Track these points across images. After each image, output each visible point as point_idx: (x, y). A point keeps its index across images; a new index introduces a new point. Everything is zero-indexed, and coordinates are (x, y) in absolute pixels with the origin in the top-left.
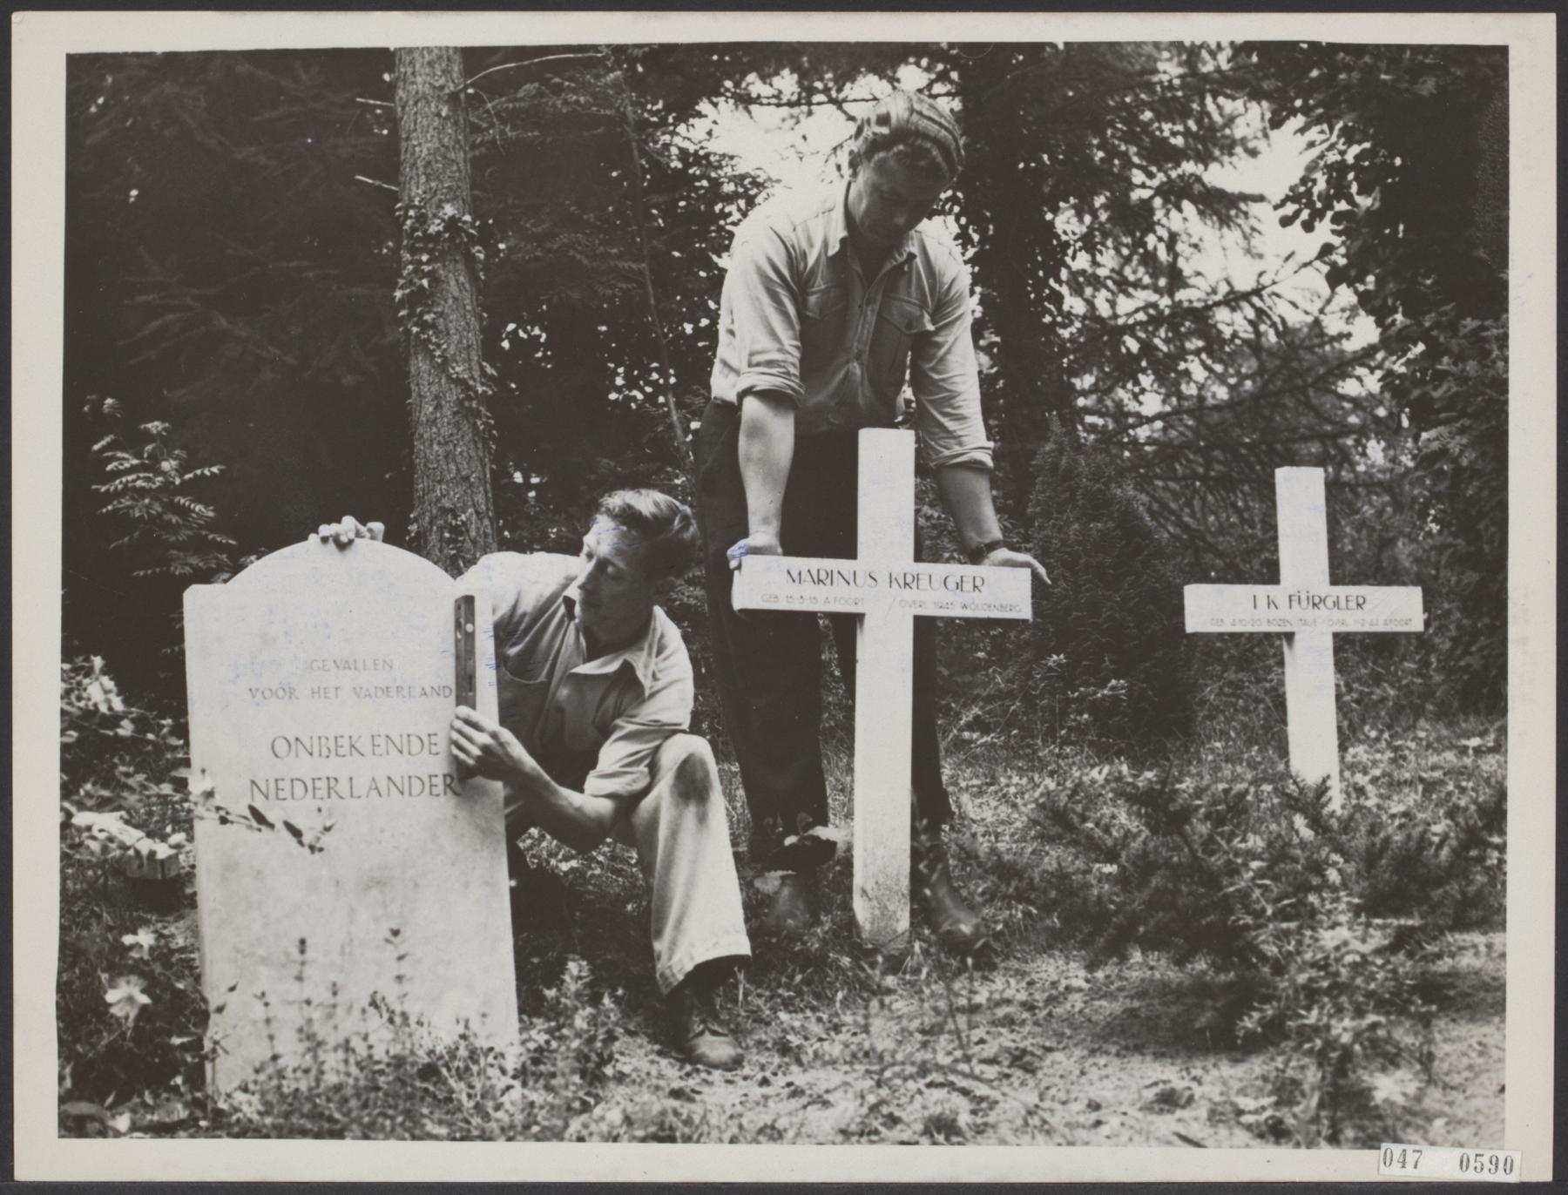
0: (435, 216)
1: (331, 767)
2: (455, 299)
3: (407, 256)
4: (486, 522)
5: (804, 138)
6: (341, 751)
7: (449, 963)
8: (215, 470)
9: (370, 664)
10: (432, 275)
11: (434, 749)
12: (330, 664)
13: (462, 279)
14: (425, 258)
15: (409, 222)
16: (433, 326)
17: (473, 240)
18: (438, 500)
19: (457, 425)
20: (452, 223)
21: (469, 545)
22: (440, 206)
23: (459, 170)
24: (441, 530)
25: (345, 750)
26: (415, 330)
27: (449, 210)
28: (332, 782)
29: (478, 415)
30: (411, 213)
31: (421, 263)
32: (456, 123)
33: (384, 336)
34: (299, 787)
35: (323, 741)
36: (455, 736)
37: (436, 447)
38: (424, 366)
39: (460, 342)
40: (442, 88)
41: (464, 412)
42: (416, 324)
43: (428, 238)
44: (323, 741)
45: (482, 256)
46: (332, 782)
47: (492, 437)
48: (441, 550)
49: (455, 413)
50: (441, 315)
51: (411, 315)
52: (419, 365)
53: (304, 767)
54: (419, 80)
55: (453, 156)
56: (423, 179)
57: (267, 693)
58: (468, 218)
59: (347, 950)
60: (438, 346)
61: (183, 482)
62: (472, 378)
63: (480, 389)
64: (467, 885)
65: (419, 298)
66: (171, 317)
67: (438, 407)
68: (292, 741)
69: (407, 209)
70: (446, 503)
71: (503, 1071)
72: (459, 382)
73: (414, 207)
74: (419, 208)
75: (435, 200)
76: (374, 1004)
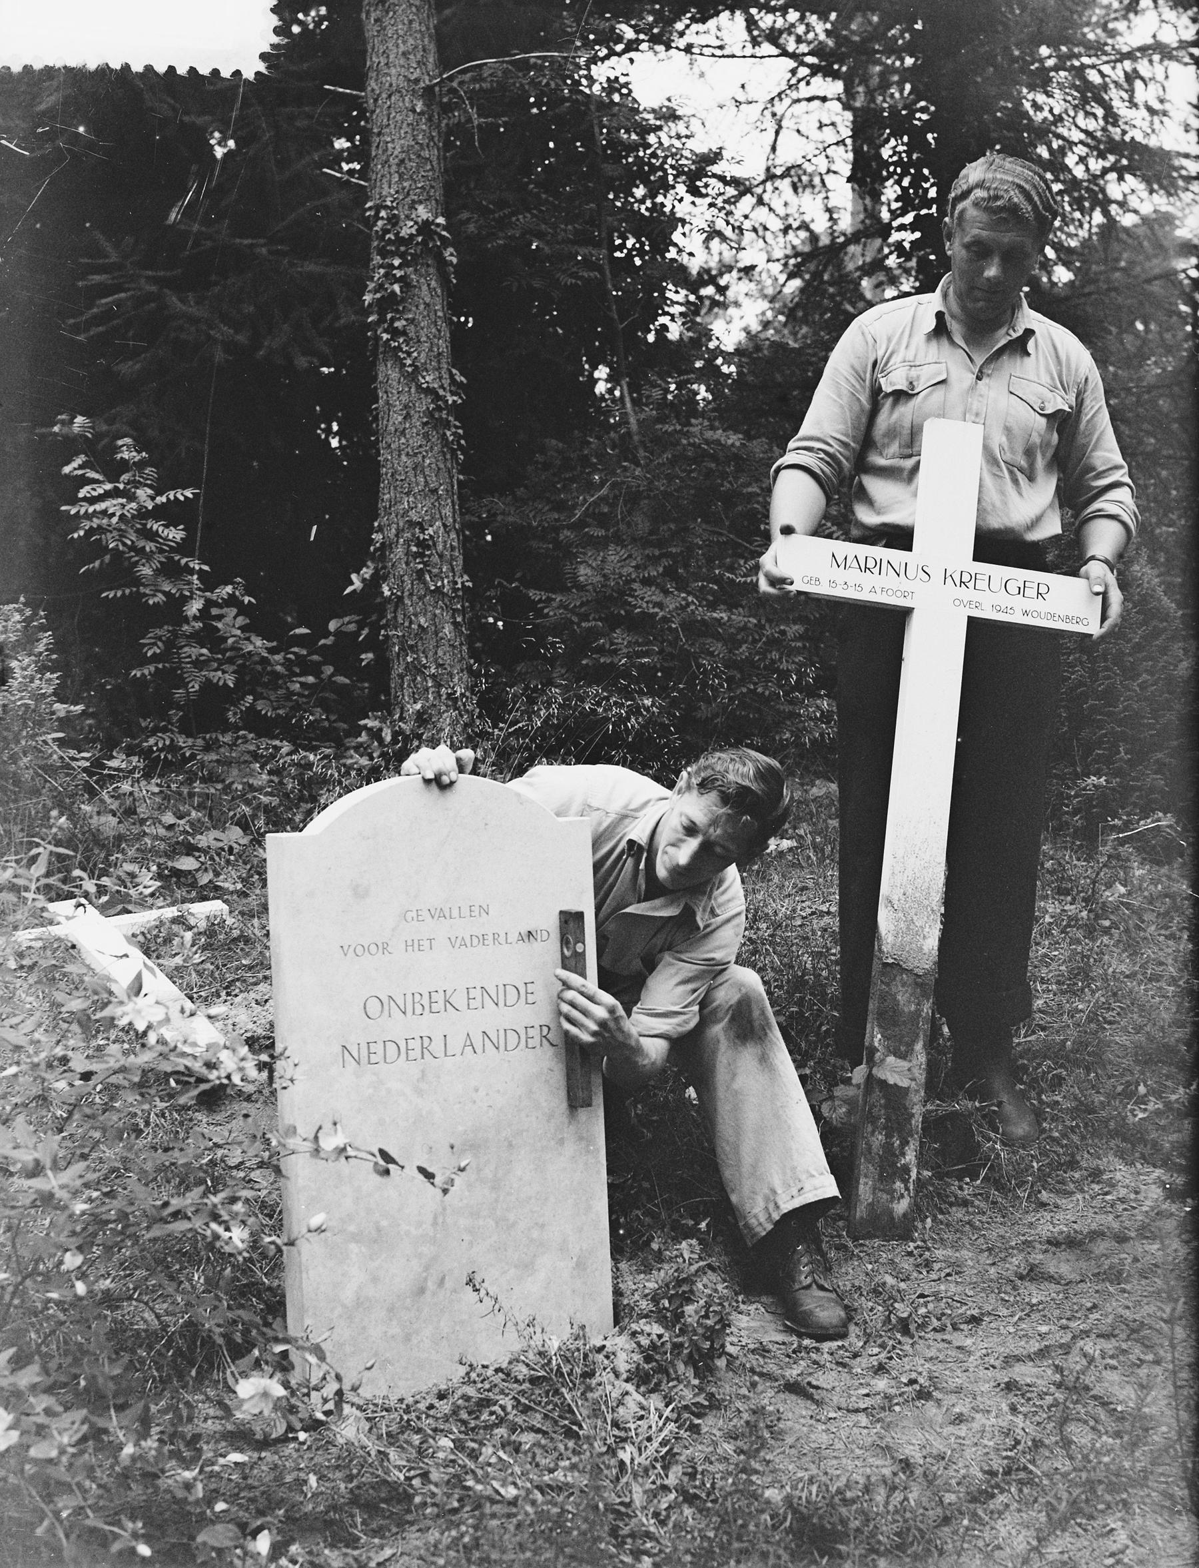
0: (408, 217)
1: (425, 1025)
2: (427, 305)
3: (377, 259)
4: (453, 535)
5: (743, 86)
6: (435, 1007)
7: (543, 1226)
8: (189, 493)
9: (465, 911)
10: (403, 280)
11: (531, 999)
12: (425, 914)
13: (433, 284)
14: (397, 262)
15: (380, 223)
16: (404, 333)
17: (445, 242)
18: (406, 512)
19: (426, 436)
20: (425, 228)
21: (436, 559)
22: (412, 207)
23: (432, 169)
24: (407, 543)
25: (439, 1006)
26: (385, 336)
27: (423, 213)
28: (426, 1040)
29: (447, 425)
30: (383, 214)
31: (392, 267)
32: (430, 119)
33: (338, 317)
34: (392, 1048)
35: (417, 997)
36: (565, 1008)
37: (404, 458)
38: (394, 375)
39: (431, 350)
40: (417, 81)
41: (434, 422)
42: (385, 331)
43: (400, 240)
44: (417, 997)
45: (455, 260)
46: (426, 1040)
47: (460, 446)
48: (407, 564)
49: (425, 424)
50: (411, 321)
51: (382, 320)
52: (388, 373)
53: (398, 1027)
54: (393, 71)
55: (426, 154)
56: (396, 178)
57: (359, 950)
58: (441, 220)
59: (440, 1220)
60: (409, 354)
61: (156, 507)
62: (442, 387)
63: (450, 399)
64: (561, 1142)
65: (388, 303)
66: (123, 295)
67: (407, 417)
68: (385, 1001)
69: (378, 208)
70: (416, 518)
71: (617, 1375)
72: (430, 391)
73: (386, 207)
74: (392, 208)
75: (408, 200)
76: (470, 1281)
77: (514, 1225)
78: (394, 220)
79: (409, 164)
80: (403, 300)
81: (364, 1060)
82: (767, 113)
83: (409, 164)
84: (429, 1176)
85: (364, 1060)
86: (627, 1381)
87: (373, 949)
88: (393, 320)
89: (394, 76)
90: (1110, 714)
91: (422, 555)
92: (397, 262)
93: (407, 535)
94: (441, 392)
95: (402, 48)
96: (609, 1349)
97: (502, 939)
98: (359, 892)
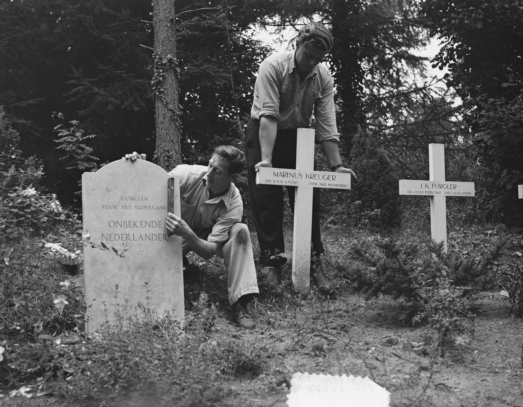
1: (127, 230)
2: (171, 84)
3: (155, 70)
4: (179, 155)
7: (163, 293)
9: (140, 199)
10: (163, 76)
13: (173, 78)
14: (161, 71)
19: (170, 124)
20: (170, 61)
21: (173, 162)
22: (166, 55)
24: (164, 157)
26: (157, 93)
27: (169, 56)
29: (177, 121)
30: (157, 57)
31: (160, 72)
34: (117, 237)
37: (163, 131)
40: (168, 17)
41: (172, 119)
42: (158, 92)
43: (162, 65)
52: (158, 105)
53: (119, 230)
54: (161, 15)
56: (161, 46)
57: (108, 207)
58: (175, 59)
59: (131, 288)
64: (169, 269)
66: (80, 87)
70: (166, 149)
71: (180, 328)
72: (171, 110)
74: (160, 55)
77: (154, 292)
78: (160, 59)
79: (165, 42)
80: (163, 82)
81: (108, 239)
82: (291, 45)
83: (165, 42)
84: (116, 251)
85: (108, 239)
86: (183, 330)
87: (112, 207)
88: (160, 88)
89: (161, 16)
90: (371, 192)
91: (168, 160)
92: (161, 71)
93: (164, 154)
94: (175, 111)
95: (164, 8)
96: (178, 321)
97: (152, 208)
98: (108, 190)
